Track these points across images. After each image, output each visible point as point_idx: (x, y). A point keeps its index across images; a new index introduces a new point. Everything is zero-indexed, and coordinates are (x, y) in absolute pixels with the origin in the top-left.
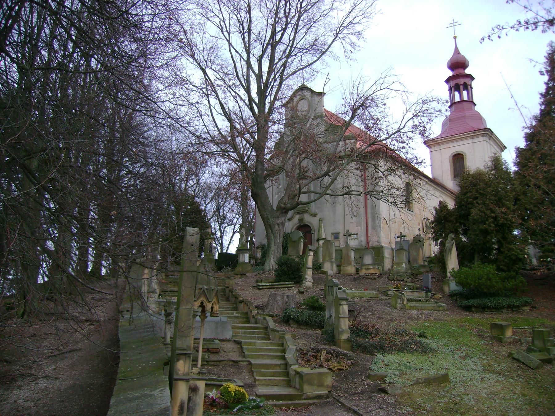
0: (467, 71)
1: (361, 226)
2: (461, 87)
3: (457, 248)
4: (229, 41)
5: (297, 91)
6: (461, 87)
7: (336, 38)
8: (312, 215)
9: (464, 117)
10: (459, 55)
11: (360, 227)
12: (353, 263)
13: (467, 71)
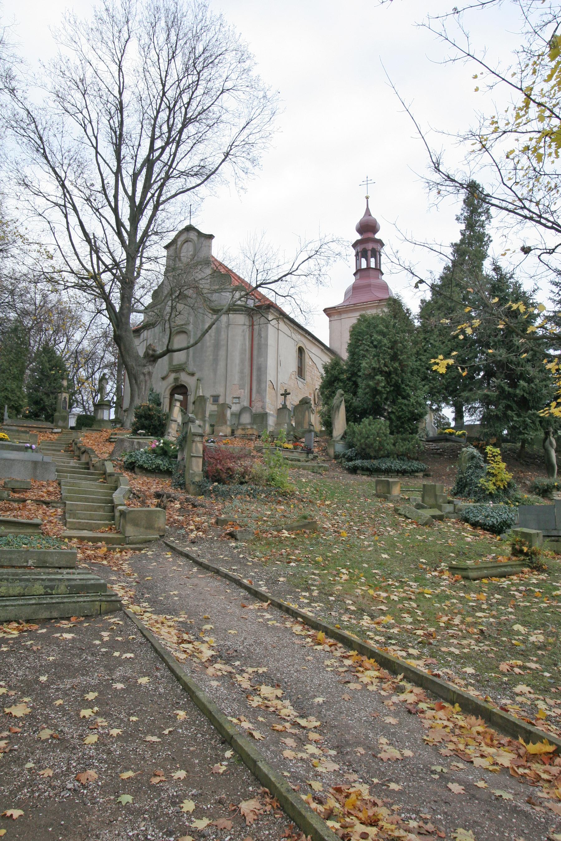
0: (377, 236)
1: (244, 389)
2: (369, 253)
3: (347, 411)
4: (96, 148)
5: (181, 233)
6: (369, 253)
7: (226, 157)
8: (189, 374)
9: (369, 286)
10: (370, 217)
11: (242, 391)
12: (228, 423)
13: (377, 236)
